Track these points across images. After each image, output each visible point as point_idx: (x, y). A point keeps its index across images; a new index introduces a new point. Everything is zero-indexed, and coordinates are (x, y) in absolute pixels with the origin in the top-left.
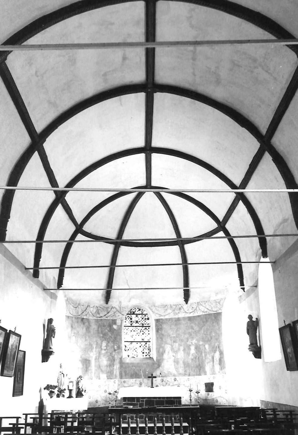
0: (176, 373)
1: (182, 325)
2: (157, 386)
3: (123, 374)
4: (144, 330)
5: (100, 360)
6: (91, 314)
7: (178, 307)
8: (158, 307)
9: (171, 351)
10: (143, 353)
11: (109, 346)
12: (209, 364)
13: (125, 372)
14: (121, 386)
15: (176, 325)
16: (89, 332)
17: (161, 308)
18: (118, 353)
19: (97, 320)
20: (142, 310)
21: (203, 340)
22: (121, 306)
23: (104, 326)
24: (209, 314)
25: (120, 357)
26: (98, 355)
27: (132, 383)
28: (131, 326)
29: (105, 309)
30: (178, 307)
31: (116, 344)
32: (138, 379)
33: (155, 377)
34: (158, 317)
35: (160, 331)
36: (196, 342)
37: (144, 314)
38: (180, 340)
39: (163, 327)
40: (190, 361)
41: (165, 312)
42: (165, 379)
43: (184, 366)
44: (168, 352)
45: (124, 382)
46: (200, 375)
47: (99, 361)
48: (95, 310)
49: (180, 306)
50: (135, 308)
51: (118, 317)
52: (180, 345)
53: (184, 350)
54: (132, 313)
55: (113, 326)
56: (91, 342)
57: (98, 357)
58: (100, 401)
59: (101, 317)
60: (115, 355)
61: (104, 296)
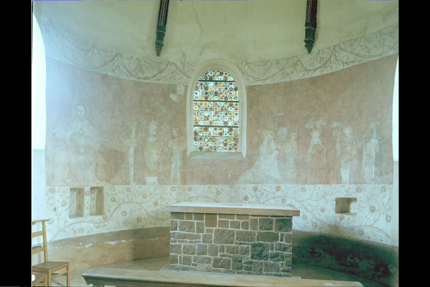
0: (278, 176)
4: (228, 107)
5: (145, 154)
6: (124, 70)
7: (291, 61)
9: (273, 141)
10: (226, 145)
20: (226, 74)
24: (360, 66)
28: (206, 100)
30: (291, 61)
32: (213, 186)
34: (252, 83)
42: (260, 187)
44: (269, 143)
45: (190, 189)
46: (328, 182)
48: (133, 66)
50: (214, 71)
51: (180, 81)
53: (298, 139)
54: (208, 79)
55: (169, 95)
58: (145, 219)
59: (148, 78)
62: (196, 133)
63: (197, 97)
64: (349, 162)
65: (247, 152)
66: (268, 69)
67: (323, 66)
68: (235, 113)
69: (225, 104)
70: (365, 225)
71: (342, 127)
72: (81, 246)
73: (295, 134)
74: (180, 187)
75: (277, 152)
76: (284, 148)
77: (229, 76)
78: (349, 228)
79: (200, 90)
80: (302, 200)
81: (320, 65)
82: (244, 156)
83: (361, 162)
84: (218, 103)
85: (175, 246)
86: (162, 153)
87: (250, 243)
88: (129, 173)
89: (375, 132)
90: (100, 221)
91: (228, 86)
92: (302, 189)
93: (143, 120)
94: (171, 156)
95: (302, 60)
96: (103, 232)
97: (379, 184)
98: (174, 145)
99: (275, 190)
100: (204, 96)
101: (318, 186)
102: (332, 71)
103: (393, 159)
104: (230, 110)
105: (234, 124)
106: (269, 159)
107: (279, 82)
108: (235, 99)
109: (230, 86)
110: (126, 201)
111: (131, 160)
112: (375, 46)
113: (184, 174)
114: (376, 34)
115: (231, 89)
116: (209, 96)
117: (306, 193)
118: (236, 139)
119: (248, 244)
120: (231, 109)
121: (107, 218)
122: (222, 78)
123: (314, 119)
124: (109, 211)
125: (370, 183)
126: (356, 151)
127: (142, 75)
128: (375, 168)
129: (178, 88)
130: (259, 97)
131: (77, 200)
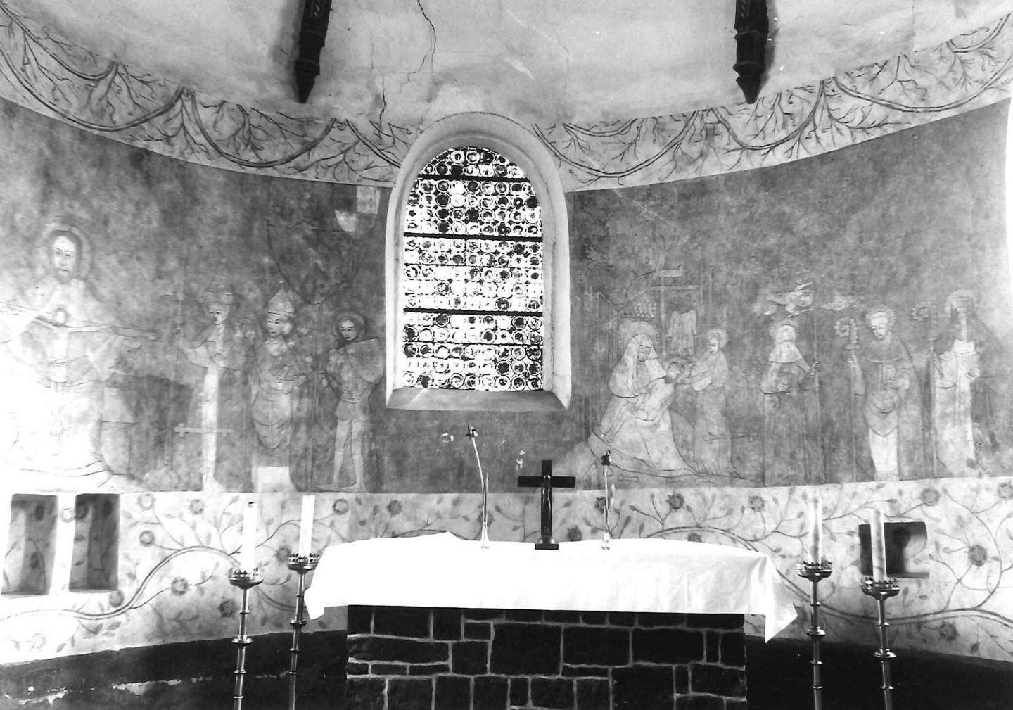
0: (672, 463)
1: (722, 217)
2: (574, 535)
3: (389, 467)
5: (254, 392)
6: (200, 139)
7: (698, 123)
8: (589, 131)
9: (653, 354)
10: (503, 368)
11: (308, 318)
12: (892, 418)
13: (399, 457)
14: (373, 527)
15: (684, 217)
16: (188, 233)
17: (602, 134)
18: (361, 356)
19: (243, 176)
20: (502, 160)
21: (856, 287)
22: (388, 117)
23: (285, 213)
24: (901, 136)
25: (371, 379)
26: (240, 360)
27: (439, 516)
28: (443, 232)
29: (292, 126)
30: (698, 123)
31: (353, 309)
33: (568, 482)
35: (593, 254)
36: (808, 300)
37: (509, 180)
38: (705, 293)
39: (611, 232)
40: (766, 405)
41: (622, 155)
43: (728, 435)
44: (640, 362)
45: (393, 508)
46: (829, 478)
47: (246, 396)
48: (227, 127)
49: (711, 118)
50: (465, 151)
51: (366, 174)
52: (706, 323)
53: (731, 346)
54: (449, 173)
55: (334, 216)
56: (194, 285)
57: (238, 374)
60: (341, 366)
61: (285, 60)
62: (410, 332)
63: (416, 226)
64: (893, 414)
65: (574, 387)
66: (630, 144)
67: (794, 137)
68: (532, 272)
69: (500, 245)
70: (959, 607)
71: (862, 310)
72: (32, 695)
73: (723, 334)
74: (363, 501)
75: (669, 389)
76: (689, 377)
77: (511, 164)
78: (908, 621)
79: (424, 201)
80: (755, 536)
81: (782, 135)
82: (565, 402)
83: (929, 412)
84: (478, 242)
85: (365, 685)
86: (306, 391)
87: (610, 668)
88: (200, 454)
89: (964, 322)
90: (103, 610)
91: (510, 195)
92: (752, 500)
93: (251, 290)
94: (335, 401)
95: (731, 120)
96: (107, 649)
97: (992, 476)
98: (346, 367)
99: (666, 507)
100: (436, 222)
101: (800, 489)
102: (821, 152)
103: (794, 622)
104: (514, 264)
105: (530, 306)
106: (643, 410)
107: (667, 181)
108: (530, 230)
109: (514, 193)
110: (187, 545)
111: (209, 411)
112: (941, 83)
113: (374, 458)
114: (941, 51)
115: (519, 203)
116: (451, 222)
117: (765, 514)
118: (535, 351)
119: (604, 673)
120: (518, 260)
121: (122, 600)
122: (490, 170)
123: (776, 288)
124: (132, 576)
125: (962, 475)
126: (910, 380)
127: (252, 154)
128: (973, 426)
129: (359, 196)
130: (608, 225)
131: (29, 539)
